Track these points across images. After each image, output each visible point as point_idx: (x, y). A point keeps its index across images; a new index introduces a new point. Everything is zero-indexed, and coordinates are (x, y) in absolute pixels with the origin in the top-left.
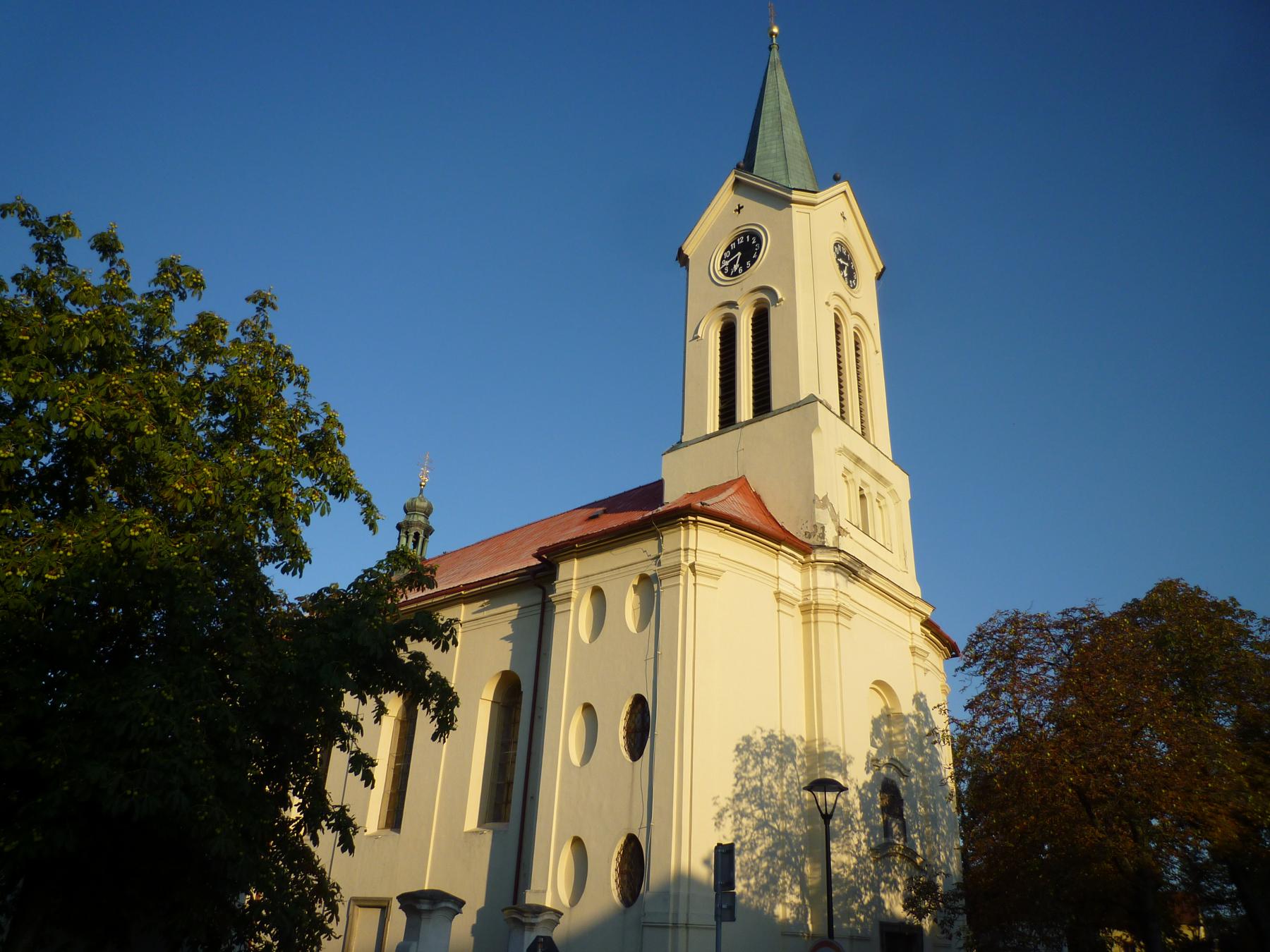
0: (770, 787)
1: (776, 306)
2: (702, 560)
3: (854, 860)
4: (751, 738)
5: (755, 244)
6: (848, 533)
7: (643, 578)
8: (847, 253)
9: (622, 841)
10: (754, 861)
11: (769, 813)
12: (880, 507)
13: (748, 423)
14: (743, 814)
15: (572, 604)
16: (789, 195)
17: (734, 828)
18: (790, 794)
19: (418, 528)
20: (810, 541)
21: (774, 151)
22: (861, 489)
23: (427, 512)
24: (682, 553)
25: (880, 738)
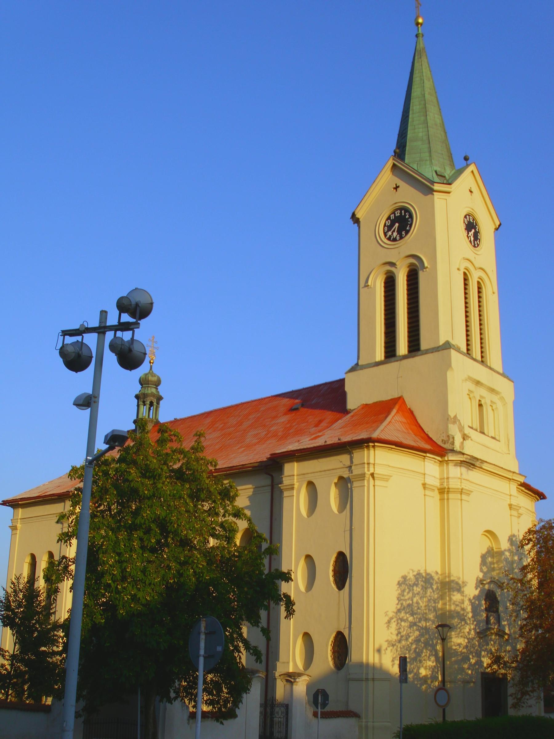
0: (417, 603)
1: (423, 271)
2: (378, 471)
3: (466, 641)
4: (407, 577)
5: (408, 218)
6: (469, 437)
7: (341, 478)
8: (473, 220)
9: (334, 635)
10: (408, 645)
11: (417, 618)
12: (493, 410)
13: (405, 357)
14: (402, 620)
15: (295, 491)
16: (432, 186)
17: (397, 628)
18: (429, 606)
19: (152, 398)
20: (445, 446)
21: (420, 134)
22: (480, 401)
23: (158, 383)
24: (366, 466)
25: (486, 566)
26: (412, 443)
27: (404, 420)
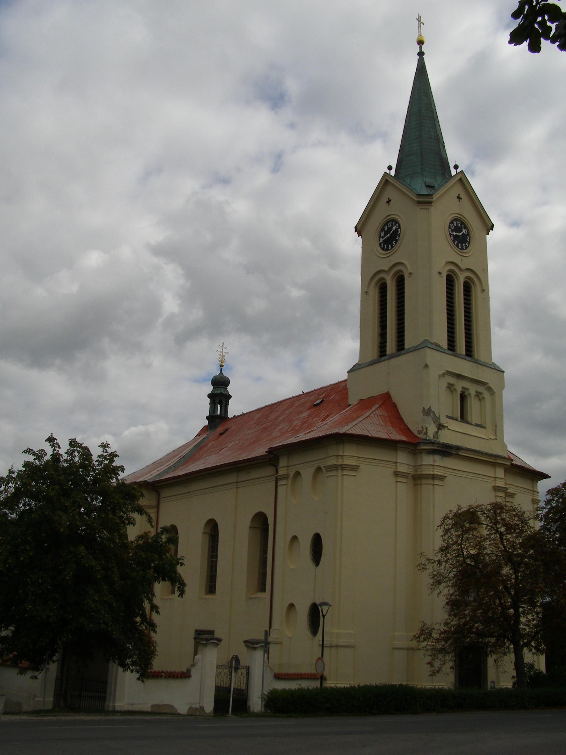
26: (383, 435)
27: (385, 414)
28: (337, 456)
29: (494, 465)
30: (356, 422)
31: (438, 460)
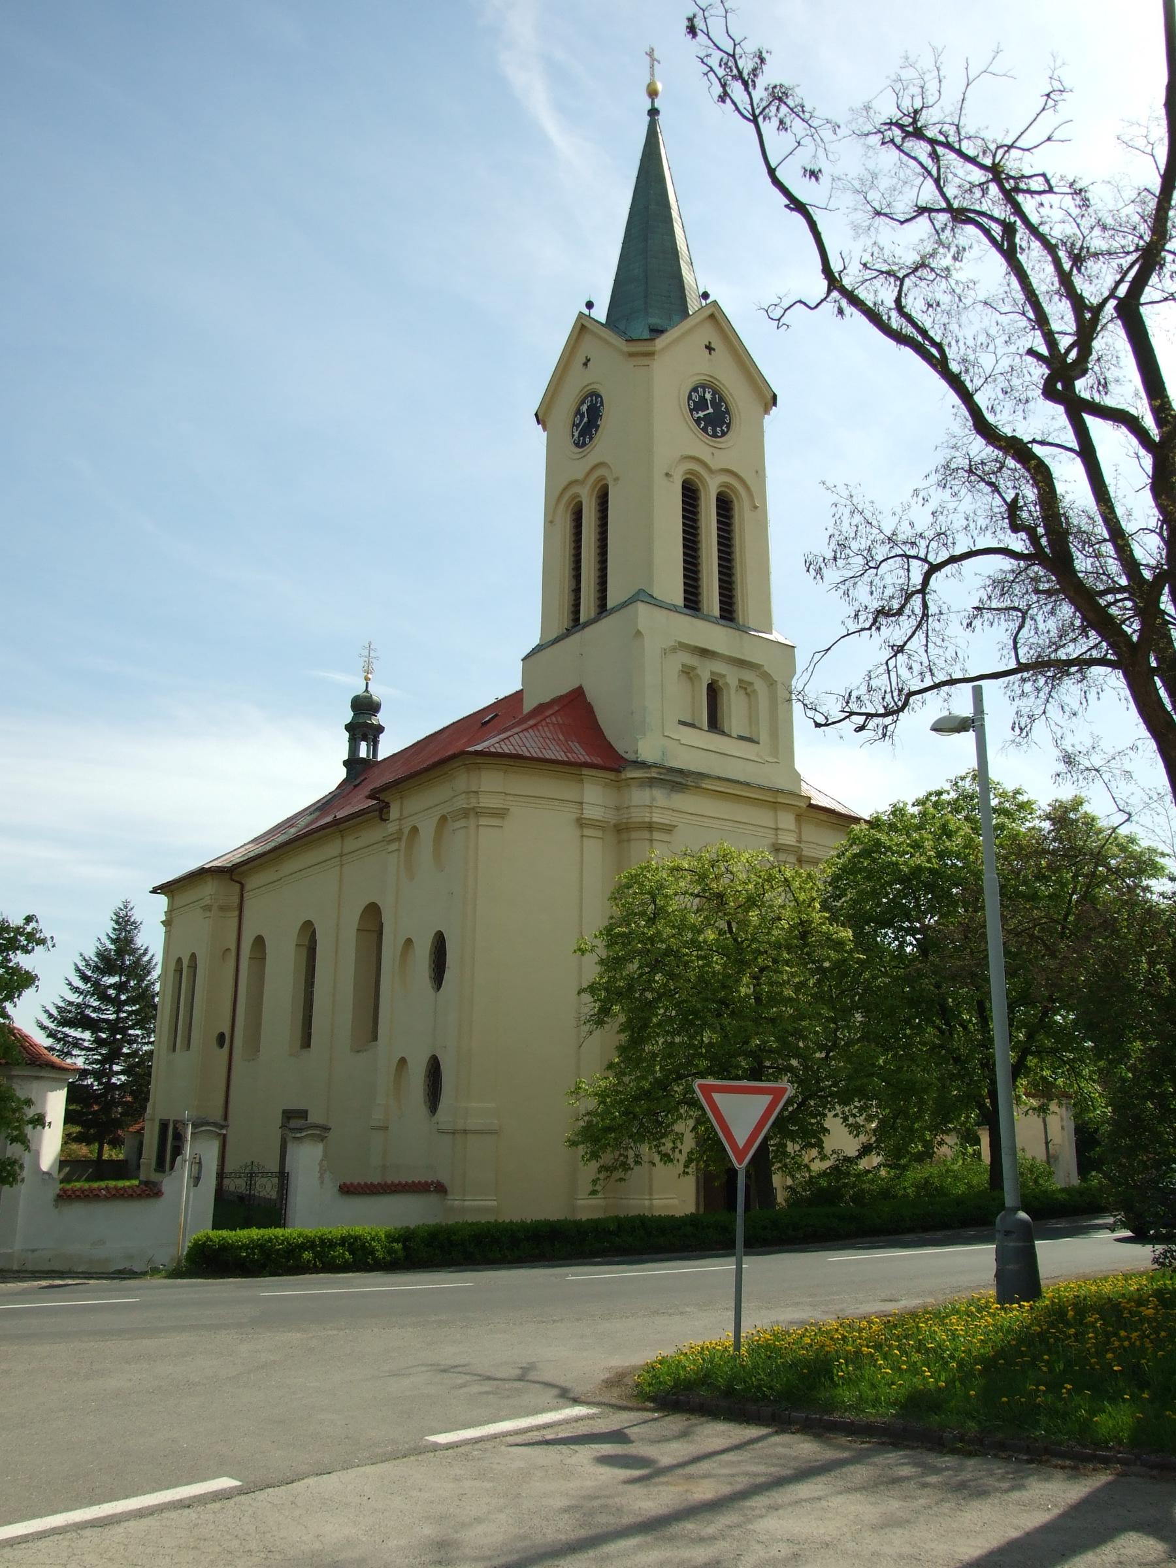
28: (468, 793)
29: (775, 806)
30: (509, 733)
31: (659, 796)
